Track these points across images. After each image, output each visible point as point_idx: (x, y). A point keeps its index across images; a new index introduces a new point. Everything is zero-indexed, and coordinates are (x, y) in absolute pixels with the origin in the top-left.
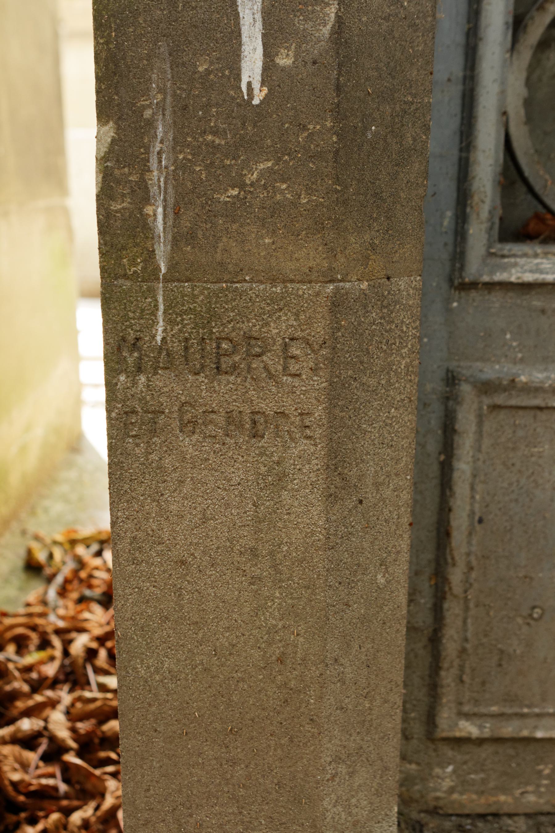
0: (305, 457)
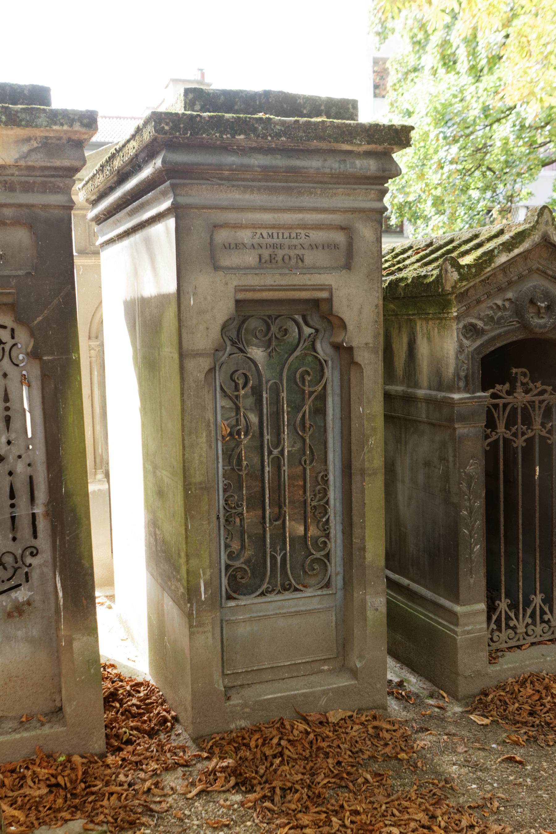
0: (210, 635)
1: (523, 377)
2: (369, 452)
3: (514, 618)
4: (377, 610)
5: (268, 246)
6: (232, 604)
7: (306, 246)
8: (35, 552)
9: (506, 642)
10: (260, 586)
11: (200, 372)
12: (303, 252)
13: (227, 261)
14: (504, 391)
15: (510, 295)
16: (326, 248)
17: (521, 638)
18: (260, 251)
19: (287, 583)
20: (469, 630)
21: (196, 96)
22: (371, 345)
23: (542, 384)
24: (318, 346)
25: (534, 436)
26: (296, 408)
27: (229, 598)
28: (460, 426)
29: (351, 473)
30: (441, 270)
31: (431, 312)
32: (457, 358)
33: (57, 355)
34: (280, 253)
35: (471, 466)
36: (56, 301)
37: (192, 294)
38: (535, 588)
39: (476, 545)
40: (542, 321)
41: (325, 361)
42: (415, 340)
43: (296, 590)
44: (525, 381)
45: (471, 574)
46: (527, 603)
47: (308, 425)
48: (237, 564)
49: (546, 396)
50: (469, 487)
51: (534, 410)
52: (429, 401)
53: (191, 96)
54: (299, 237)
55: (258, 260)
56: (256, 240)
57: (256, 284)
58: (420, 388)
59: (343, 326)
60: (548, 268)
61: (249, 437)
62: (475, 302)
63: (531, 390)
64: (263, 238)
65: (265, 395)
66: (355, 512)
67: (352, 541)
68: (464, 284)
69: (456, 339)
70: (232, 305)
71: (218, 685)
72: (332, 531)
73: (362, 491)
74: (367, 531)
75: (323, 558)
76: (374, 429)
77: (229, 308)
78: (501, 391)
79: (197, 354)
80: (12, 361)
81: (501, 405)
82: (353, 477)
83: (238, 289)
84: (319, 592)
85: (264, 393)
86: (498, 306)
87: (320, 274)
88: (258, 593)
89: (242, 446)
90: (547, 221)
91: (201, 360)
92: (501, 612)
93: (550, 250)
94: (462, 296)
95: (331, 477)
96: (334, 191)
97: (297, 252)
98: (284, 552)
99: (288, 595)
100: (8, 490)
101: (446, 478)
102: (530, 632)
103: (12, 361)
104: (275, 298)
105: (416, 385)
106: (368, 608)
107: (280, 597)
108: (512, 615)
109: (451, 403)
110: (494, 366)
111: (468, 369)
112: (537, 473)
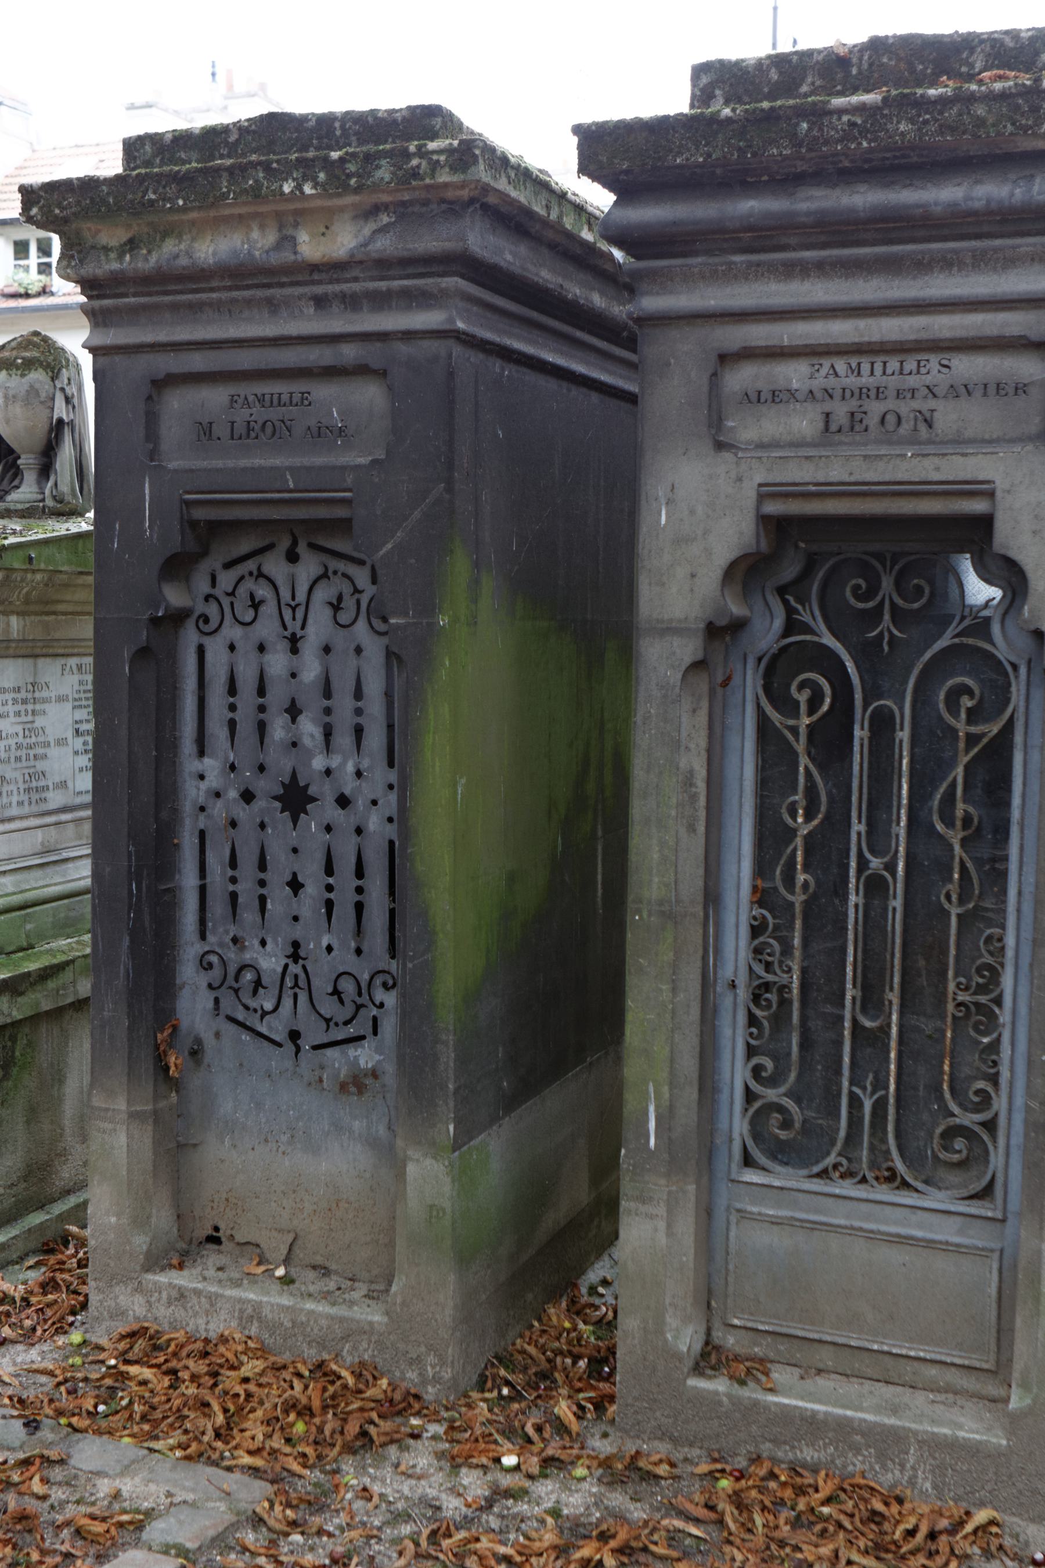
0: (662, 1225)
5: (848, 394)
6: (751, 1176)
8: (391, 982)
12: (932, 403)
16: (992, 390)
18: (828, 406)
33: (414, 617)
34: (875, 408)
36: (417, 514)
37: (663, 501)
41: (760, 659)
48: (771, 1094)
53: (705, 80)
54: (923, 370)
55: (821, 425)
56: (819, 382)
57: (807, 479)
61: (815, 822)
64: (836, 375)
65: (857, 733)
77: (741, 533)
79: (667, 630)
80: (372, 627)
85: (857, 727)
88: (816, 1169)
89: (799, 841)
91: (676, 641)
97: (916, 404)
98: (883, 1092)
100: (353, 860)
103: (372, 627)
107: (860, 1192)
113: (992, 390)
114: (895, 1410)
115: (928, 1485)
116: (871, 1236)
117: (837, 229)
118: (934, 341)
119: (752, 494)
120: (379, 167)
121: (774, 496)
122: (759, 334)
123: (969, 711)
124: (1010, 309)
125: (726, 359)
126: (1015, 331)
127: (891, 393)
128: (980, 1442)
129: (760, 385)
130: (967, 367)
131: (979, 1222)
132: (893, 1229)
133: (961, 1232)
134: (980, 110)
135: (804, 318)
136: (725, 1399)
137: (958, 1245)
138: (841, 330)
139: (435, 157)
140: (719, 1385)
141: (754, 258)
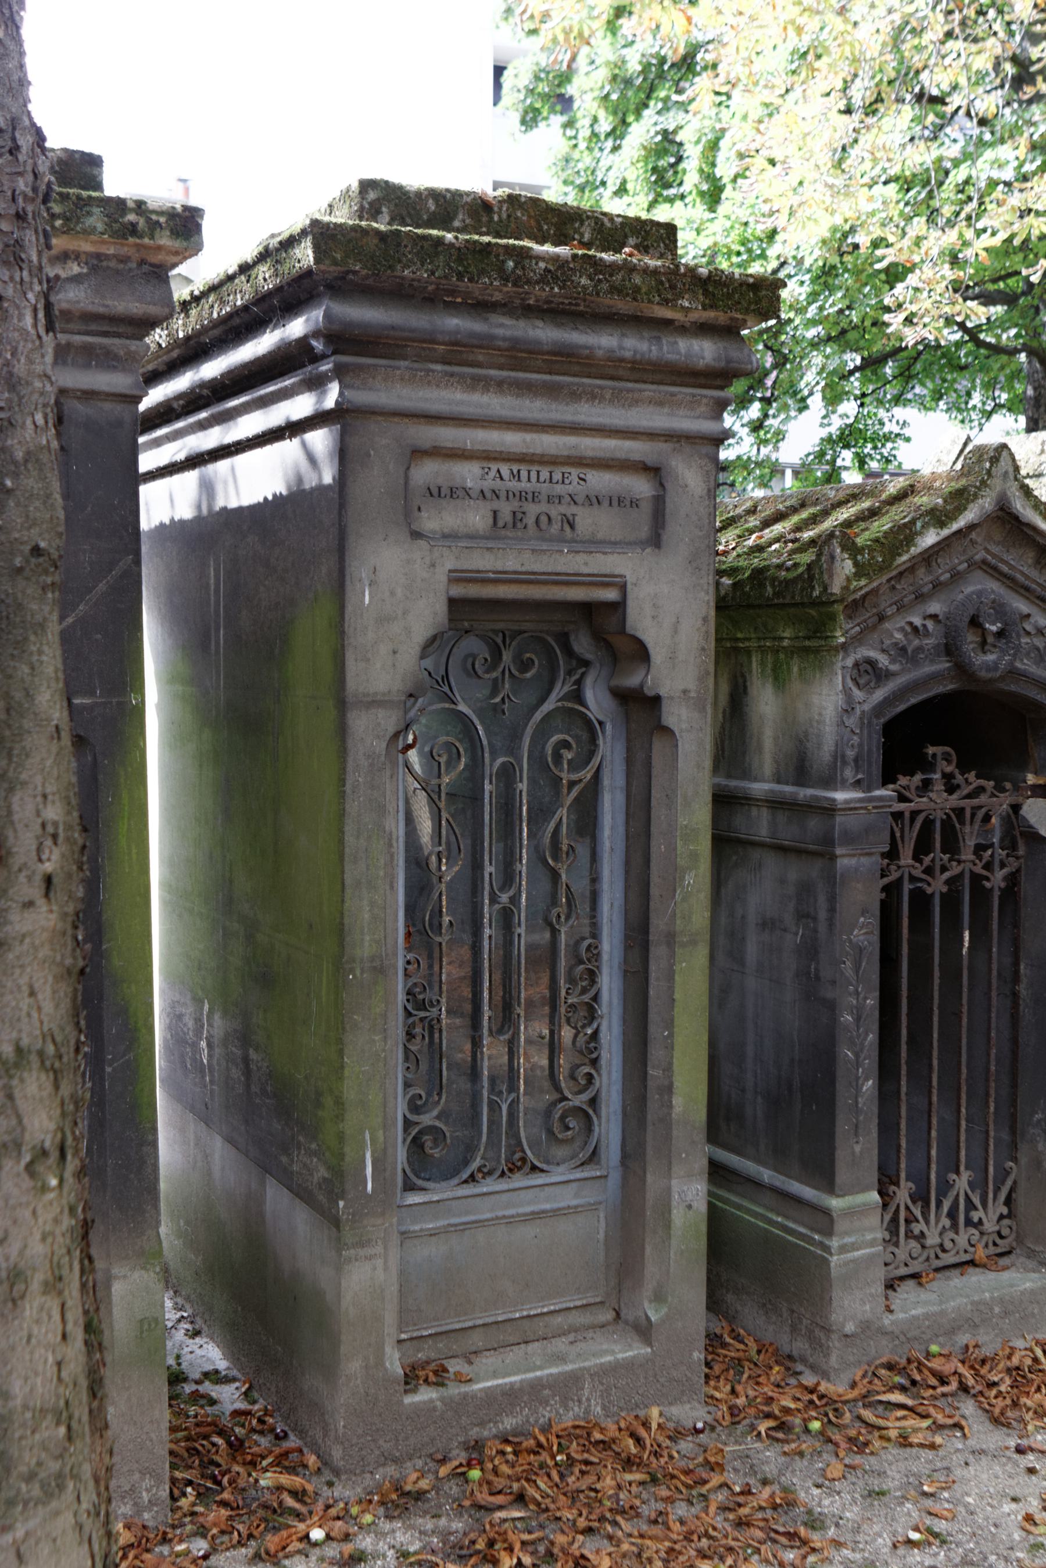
0: (379, 1262)
1: (945, 763)
2: (684, 900)
3: (920, 1218)
4: (690, 1207)
7: (580, 499)
9: (906, 1265)
10: (466, 1163)
11: (378, 737)
12: (574, 509)
13: (431, 521)
14: (913, 788)
15: (935, 607)
16: (615, 503)
17: (933, 1256)
18: (496, 505)
19: (518, 1156)
20: (853, 1244)
21: (378, 195)
22: (693, 694)
23: (978, 777)
24: (589, 695)
25: (961, 875)
26: (540, 814)
27: (409, 1187)
28: (844, 852)
29: (647, 941)
30: (819, 555)
31: (786, 634)
32: (841, 723)
34: (533, 510)
35: (862, 928)
36: (102, 587)
37: (367, 583)
38: (958, 1160)
39: (867, 1079)
40: (991, 657)
41: (601, 723)
42: (745, 688)
43: (534, 1168)
44: (949, 769)
45: (856, 1134)
46: (945, 1187)
47: (565, 848)
48: (427, 1119)
49: (983, 799)
50: (857, 969)
51: (962, 823)
52: (777, 804)
53: (372, 195)
54: (567, 481)
55: (491, 521)
56: (489, 484)
57: (488, 568)
58: (756, 780)
59: (641, 653)
60: (1002, 561)
62: (876, 618)
63: (958, 786)
64: (501, 478)
65: (487, 787)
66: (653, 1015)
67: (646, 1073)
68: (863, 582)
69: (840, 687)
70: (441, 608)
71: (392, 1364)
72: (605, 1055)
73: (670, 976)
74: (677, 1054)
75: (585, 1107)
76: (694, 856)
77: (436, 614)
78: (906, 788)
79: (374, 703)
81: (907, 815)
82: (652, 949)
83: (457, 577)
84: (579, 1174)
85: (487, 782)
86: (915, 629)
87: (605, 553)
88: (465, 1175)
90: (1006, 472)
91: (381, 713)
92: (898, 1206)
93: (1008, 527)
94: (854, 607)
95: (606, 946)
96: (636, 395)
97: (563, 509)
99: (519, 1180)
101: (810, 950)
102: (948, 1245)
104: (521, 597)
105: (746, 774)
106: (674, 1203)
107: (502, 1185)
108: (917, 1212)
109: (830, 810)
110: (903, 742)
111: (861, 745)
112: (966, 944)
113: (615, 503)
114: (561, 1359)
115: (599, 1409)
116: (510, 1221)
117: (519, 355)
118: (580, 458)
119: (444, 579)
120: (89, 214)
121: (458, 580)
122: (447, 435)
123: (570, 762)
124: (634, 439)
125: (419, 453)
126: (636, 457)
127: (543, 497)
128: (634, 1357)
129: (440, 481)
130: (600, 481)
131: (589, 1182)
132: (528, 1209)
133: (577, 1195)
134: (637, 280)
135: (483, 427)
136: (438, 1403)
137: (576, 1207)
138: (512, 440)
139: (154, 217)
140: (426, 1395)
141: (447, 368)
